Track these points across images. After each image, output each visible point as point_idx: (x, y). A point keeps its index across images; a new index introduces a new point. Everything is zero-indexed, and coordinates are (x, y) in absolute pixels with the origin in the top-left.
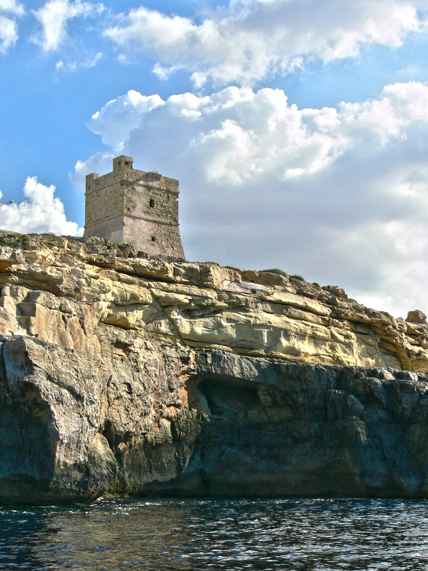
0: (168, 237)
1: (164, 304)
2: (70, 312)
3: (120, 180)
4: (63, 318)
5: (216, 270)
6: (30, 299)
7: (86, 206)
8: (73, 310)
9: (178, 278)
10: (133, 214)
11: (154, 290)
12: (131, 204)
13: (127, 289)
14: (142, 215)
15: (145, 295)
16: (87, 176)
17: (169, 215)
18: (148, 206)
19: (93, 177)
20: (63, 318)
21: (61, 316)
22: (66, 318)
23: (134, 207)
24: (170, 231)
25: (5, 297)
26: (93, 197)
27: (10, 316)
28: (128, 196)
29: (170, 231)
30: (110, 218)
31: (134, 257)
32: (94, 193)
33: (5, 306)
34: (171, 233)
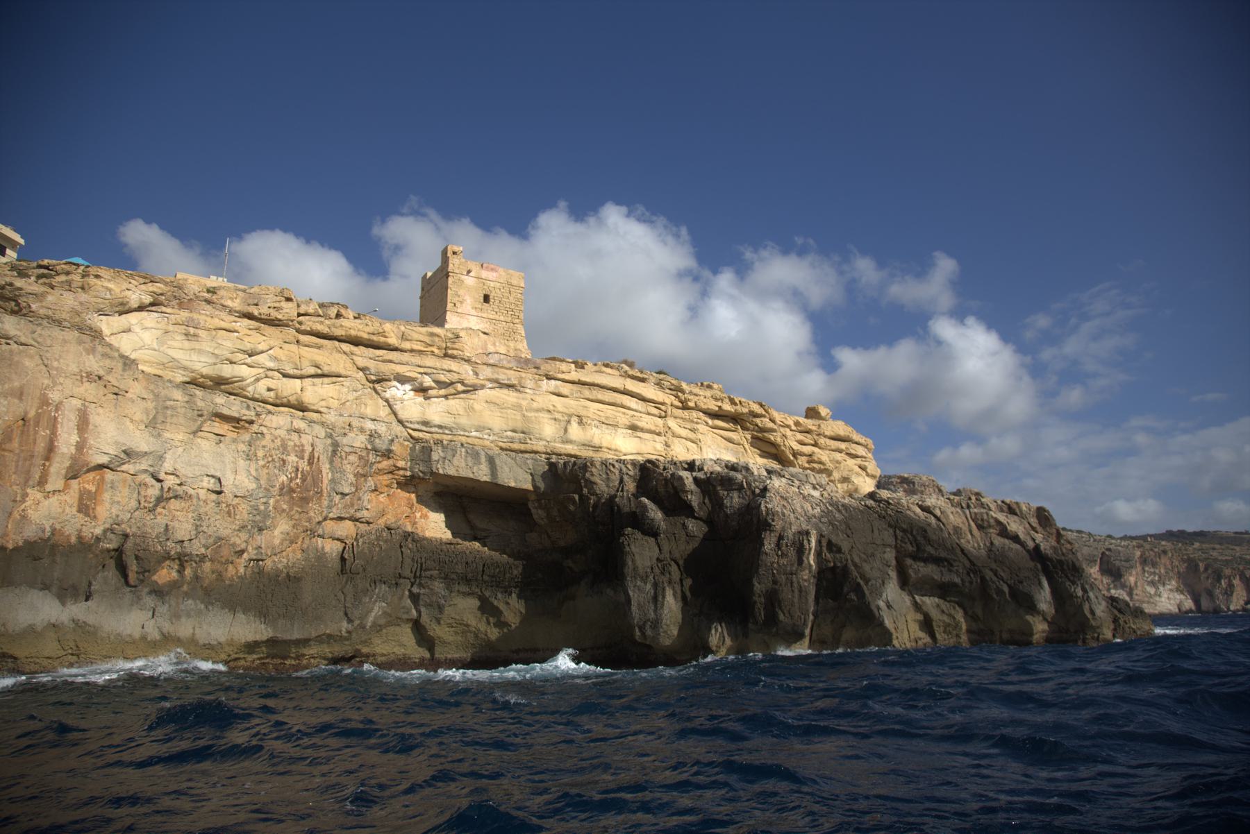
1: (373, 378)
14: (473, 312)
23: (461, 303)
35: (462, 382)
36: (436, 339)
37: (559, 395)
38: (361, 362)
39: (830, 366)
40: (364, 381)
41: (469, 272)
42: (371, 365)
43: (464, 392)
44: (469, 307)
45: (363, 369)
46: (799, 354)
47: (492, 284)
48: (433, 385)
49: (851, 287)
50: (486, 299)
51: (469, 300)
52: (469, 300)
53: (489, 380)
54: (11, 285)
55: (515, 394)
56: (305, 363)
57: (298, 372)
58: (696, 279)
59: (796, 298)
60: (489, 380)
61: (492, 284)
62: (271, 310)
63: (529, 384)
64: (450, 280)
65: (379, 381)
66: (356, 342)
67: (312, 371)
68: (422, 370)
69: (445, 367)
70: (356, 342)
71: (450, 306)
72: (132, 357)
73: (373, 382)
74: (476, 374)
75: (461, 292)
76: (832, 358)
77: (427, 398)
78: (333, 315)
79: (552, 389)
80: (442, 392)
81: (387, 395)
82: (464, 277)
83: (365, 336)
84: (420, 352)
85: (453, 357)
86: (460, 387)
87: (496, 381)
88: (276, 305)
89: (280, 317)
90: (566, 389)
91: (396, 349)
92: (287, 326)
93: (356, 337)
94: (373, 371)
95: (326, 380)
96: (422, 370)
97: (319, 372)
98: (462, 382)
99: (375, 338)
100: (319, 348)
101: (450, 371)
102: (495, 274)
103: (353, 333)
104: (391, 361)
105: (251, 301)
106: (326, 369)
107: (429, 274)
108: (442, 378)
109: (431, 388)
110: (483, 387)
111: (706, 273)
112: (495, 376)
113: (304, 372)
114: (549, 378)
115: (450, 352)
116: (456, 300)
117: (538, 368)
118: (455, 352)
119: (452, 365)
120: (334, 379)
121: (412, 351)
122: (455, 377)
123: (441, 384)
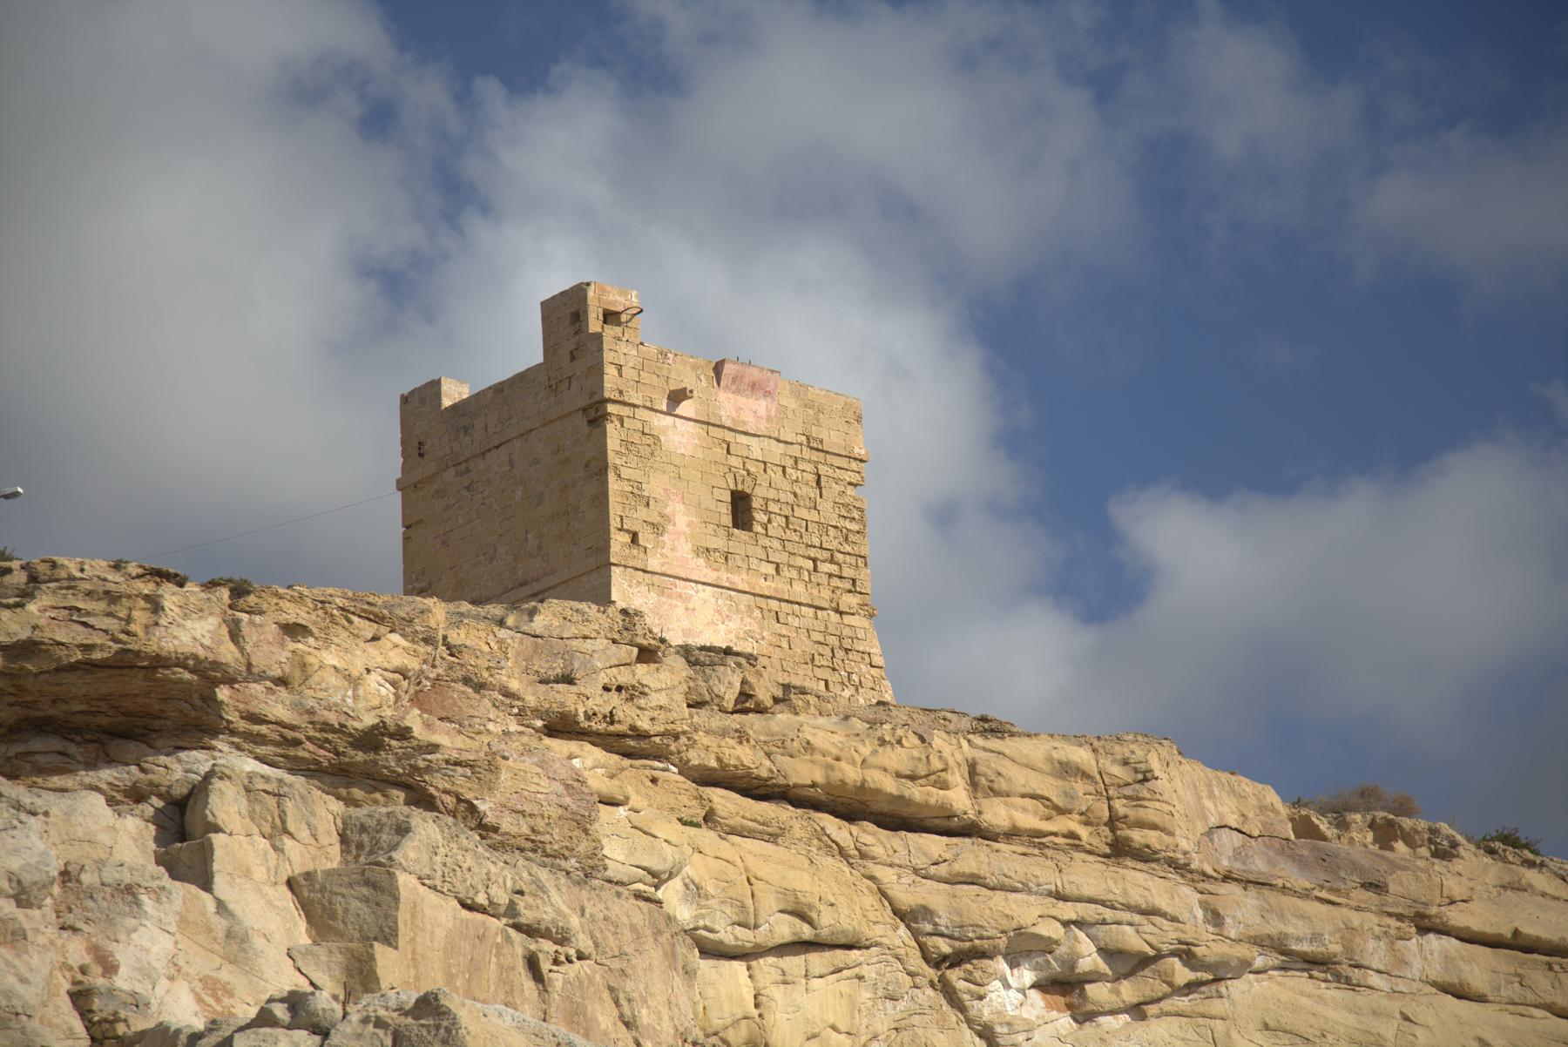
0: (826, 674)
1: (945, 947)
2: (563, 939)
3: (583, 402)
4: (532, 963)
5: (1173, 769)
6: (368, 853)
7: (406, 539)
8: (575, 921)
9: (997, 814)
10: (654, 563)
11: (886, 875)
12: (642, 513)
13: (762, 870)
14: (700, 568)
15: (845, 905)
16: (405, 400)
17: (825, 567)
18: (727, 520)
19: (438, 395)
20: (532, 963)
21: (519, 951)
22: (545, 966)
23: (658, 529)
24: (833, 641)
25: (218, 839)
26: (440, 493)
27: (258, 942)
28: (625, 473)
29: (833, 641)
30: (537, 587)
31: (760, 710)
32: (449, 475)
33: (219, 882)
34: (840, 654)
35: (1186, 954)
36: (1080, 787)
37: (1461, 993)
38: (908, 893)
39: (1099, 585)
40: (916, 961)
41: (677, 397)
42: (932, 895)
43: (1191, 987)
44: (685, 549)
45: (905, 916)
46: (944, 516)
47: (756, 448)
48: (1103, 967)
49: (1168, 174)
50: (741, 509)
51: (682, 519)
52: (682, 519)
53: (1258, 941)
54: (403, 734)
55: (1334, 993)
56: (769, 903)
57: (746, 937)
58: (379, 120)
59: (892, 225)
60: (1258, 941)
61: (756, 448)
62: (615, 699)
63: (1375, 952)
64: (614, 436)
65: (956, 960)
66: (851, 806)
67: (785, 929)
68: (1069, 911)
69: (1136, 897)
70: (851, 806)
71: (618, 541)
72: (162, 869)
73: (938, 962)
74: (1215, 918)
75: (655, 486)
76: (1108, 535)
77: (1084, 1017)
78: (730, 698)
79: (1436, 972)
80: (1129, 991)
81: (984, 1011)
82: (661, 422)
83: (890, 785)
84: (1035, 837)
85: (1145, 856)
86: (1183, 975)
87: (1277, 945)
88: (624, 677)
89: (644, 724)
90: (1478, 968)
91: (971, 830)
92: (660, 755)
93: (862, 787)
94: (943, 922)
95: (817, 961)
96: (1069, 911)
97: (807, 932)
98: (1186, 954)
99: (916, 792)
100: (773, 838)
101: (1150, 912)
102: (762, 406)
103: (851, 774)
104: (973, 880)
105: (542, 666)
106: (827, 921)
107: (454, 392)
108: (1131, 939)
109: (1093, 977)
110: (1245, 966)
111: (426, 93)
112: (1274, 927)
113: (761, 936)
114: (1426, 925)
115: (1137, 836)
116: (637, 518)
117: (1376, 887)
118: (1153, 838)
119: (1138, 883)
120: (840, 956)
121: (1013, 834)
122: (1164, 935)
123: (1128, 963)
